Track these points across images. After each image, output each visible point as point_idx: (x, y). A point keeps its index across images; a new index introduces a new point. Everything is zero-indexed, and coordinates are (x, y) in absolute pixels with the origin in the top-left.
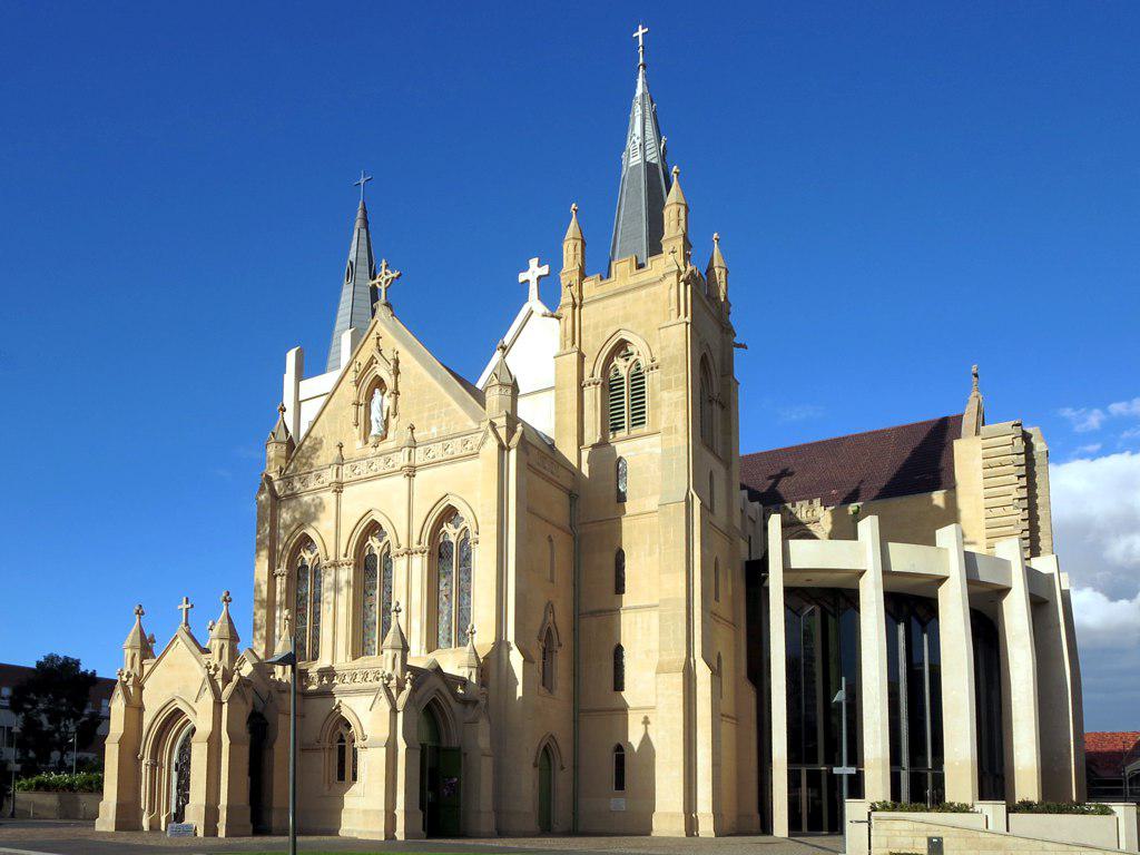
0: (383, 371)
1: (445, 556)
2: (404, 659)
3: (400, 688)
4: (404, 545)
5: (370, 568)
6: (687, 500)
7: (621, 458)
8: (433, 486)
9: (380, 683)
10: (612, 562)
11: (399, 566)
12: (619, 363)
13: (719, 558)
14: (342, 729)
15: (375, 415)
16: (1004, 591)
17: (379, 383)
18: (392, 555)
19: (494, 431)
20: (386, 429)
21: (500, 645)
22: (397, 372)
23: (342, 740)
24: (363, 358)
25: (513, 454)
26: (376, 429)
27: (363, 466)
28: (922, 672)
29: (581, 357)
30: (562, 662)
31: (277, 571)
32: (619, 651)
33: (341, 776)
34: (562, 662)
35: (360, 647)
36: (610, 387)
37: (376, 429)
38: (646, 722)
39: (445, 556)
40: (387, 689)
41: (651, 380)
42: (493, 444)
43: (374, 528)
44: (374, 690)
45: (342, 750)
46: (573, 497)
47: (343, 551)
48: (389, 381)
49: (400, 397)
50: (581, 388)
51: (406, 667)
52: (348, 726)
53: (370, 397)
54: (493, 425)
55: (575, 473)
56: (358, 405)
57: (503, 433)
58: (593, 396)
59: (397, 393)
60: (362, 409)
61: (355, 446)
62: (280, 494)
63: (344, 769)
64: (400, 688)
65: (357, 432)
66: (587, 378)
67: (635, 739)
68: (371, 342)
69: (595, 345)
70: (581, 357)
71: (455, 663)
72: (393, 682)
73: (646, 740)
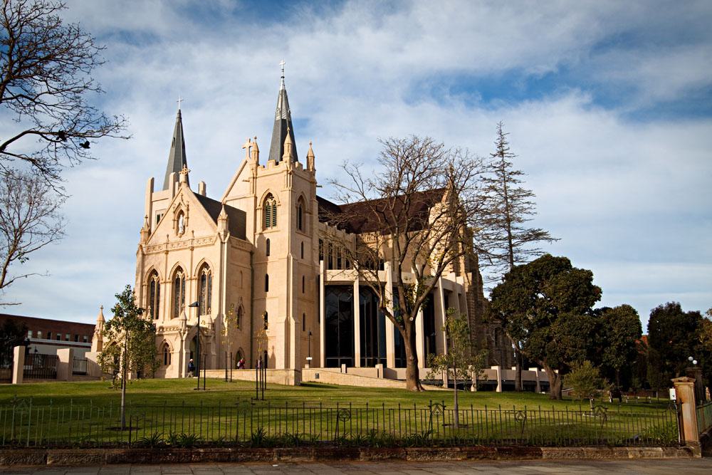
0: (184, 209)
1: (203, 279)
2: (186, 323)
3: (184, 333)
4: (189, 277)
5: (177, 284)
6: (288, 257)
7: (268, 239)
8: (199, 256)
9: (177, 332)
10: (264, 278)
11: (188, 284)
12: (269, 200)
13: (306, 314)
14: (166, 347)
15: (180, 225)
16: (386, 283)
17: (182, 212)
18: (185, 279)
19: (220, 236)
20: (184, 230)
21: (220, 315)
22: (188, 210)
23: (166, 351)
24: (177, 203)
25: (226, 245)
26: (181, 231)
27: (176, 245)
28: (380, 352)
29: (256, 198)
30: (246, 319)
31: (144, 284)
32: (267, 277)
33: (166, 364)
34: (246, 319)
35: (175, 314)
36: (266, 209)
37: (181, 231)
38: (273, 348)
39: (203, 279)
40: (180, 333)
41: (279, 209)
42: (218, 242)
43: (179, 269)
44: (177, 334)
45: (166, 354)
46: (252, 253)
47: (168, 278)
48: (185, 212)
49: (189, 219)
50: (256, 210)
51: (187, 326)
52: (168, 346)
53: (179, 217)
54: (219, 234)
55: (253, 246)
56: (174, 220)
57: (222, 237)
58: (259, 213)
59: (188, 218)
60: (176, 222)
61: (173, 238)
62: (145, 253)
63: (167, 361)
64: (184, 333)
65: (174, 231)
66: (258, 207)
67: (270, 354)
68: (179, 197)
69: (261, 194)
70: (256, 198)
71: (205, 322)
72: (182, 332)
73: (273, 355)
